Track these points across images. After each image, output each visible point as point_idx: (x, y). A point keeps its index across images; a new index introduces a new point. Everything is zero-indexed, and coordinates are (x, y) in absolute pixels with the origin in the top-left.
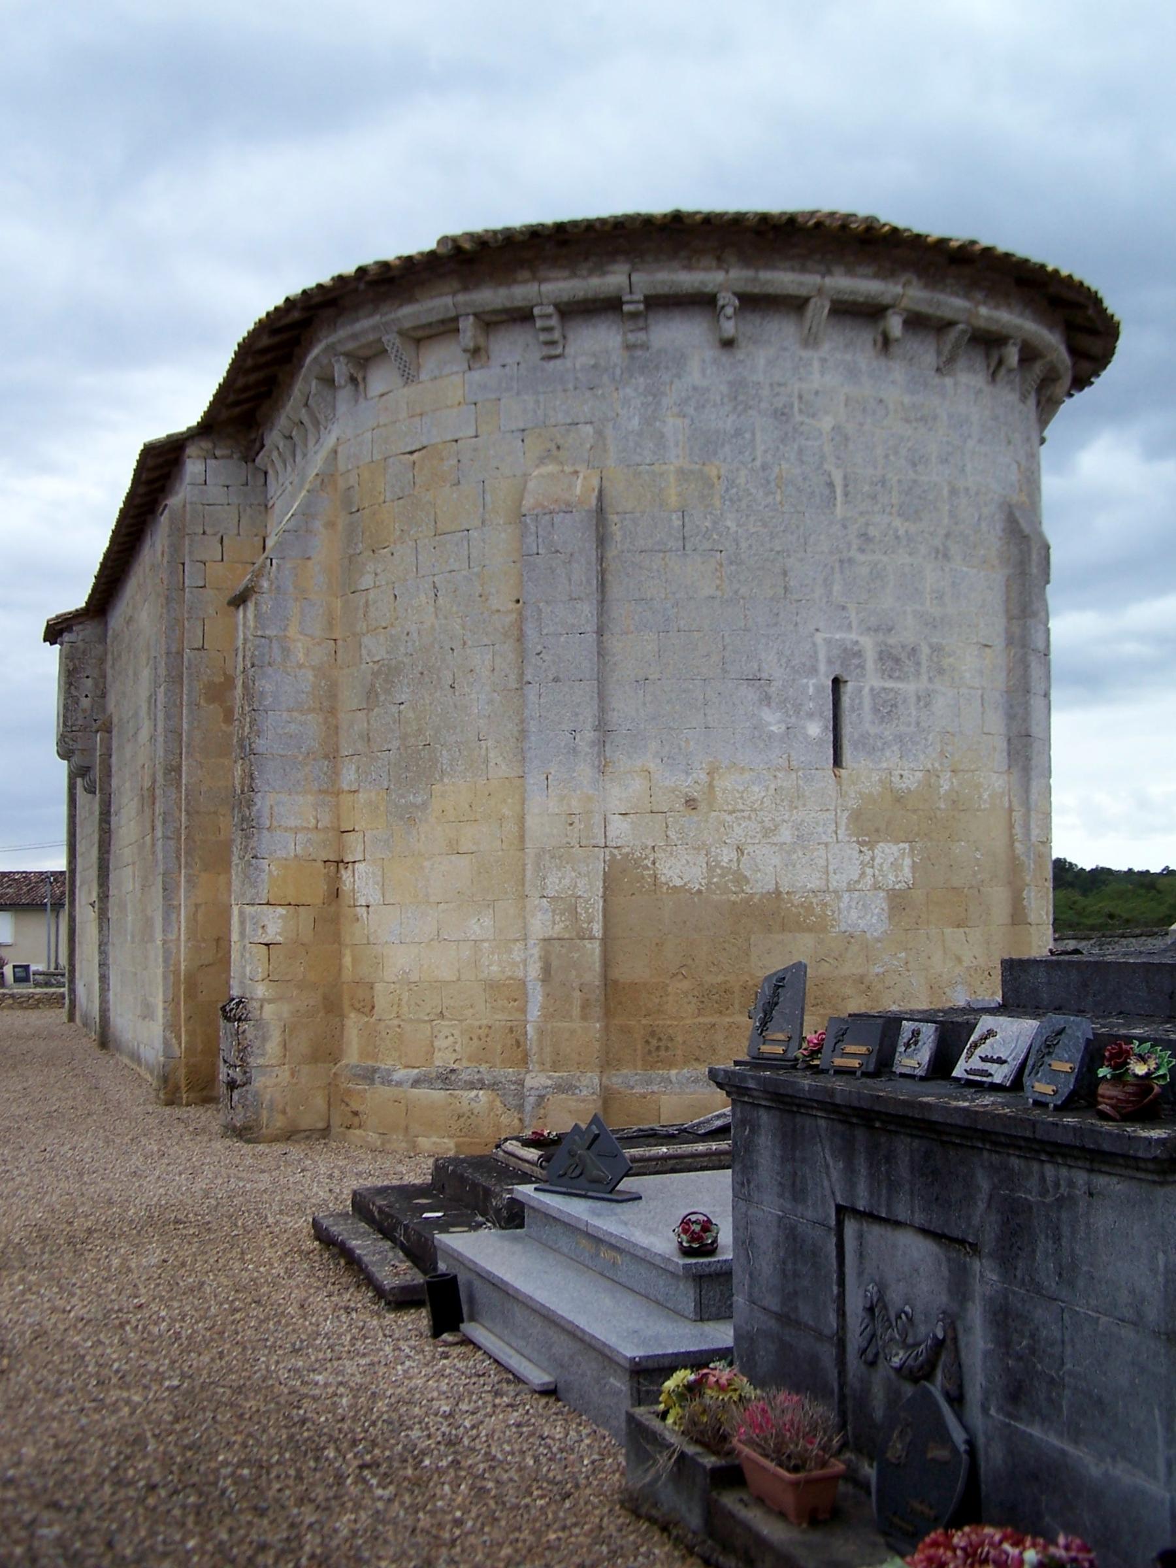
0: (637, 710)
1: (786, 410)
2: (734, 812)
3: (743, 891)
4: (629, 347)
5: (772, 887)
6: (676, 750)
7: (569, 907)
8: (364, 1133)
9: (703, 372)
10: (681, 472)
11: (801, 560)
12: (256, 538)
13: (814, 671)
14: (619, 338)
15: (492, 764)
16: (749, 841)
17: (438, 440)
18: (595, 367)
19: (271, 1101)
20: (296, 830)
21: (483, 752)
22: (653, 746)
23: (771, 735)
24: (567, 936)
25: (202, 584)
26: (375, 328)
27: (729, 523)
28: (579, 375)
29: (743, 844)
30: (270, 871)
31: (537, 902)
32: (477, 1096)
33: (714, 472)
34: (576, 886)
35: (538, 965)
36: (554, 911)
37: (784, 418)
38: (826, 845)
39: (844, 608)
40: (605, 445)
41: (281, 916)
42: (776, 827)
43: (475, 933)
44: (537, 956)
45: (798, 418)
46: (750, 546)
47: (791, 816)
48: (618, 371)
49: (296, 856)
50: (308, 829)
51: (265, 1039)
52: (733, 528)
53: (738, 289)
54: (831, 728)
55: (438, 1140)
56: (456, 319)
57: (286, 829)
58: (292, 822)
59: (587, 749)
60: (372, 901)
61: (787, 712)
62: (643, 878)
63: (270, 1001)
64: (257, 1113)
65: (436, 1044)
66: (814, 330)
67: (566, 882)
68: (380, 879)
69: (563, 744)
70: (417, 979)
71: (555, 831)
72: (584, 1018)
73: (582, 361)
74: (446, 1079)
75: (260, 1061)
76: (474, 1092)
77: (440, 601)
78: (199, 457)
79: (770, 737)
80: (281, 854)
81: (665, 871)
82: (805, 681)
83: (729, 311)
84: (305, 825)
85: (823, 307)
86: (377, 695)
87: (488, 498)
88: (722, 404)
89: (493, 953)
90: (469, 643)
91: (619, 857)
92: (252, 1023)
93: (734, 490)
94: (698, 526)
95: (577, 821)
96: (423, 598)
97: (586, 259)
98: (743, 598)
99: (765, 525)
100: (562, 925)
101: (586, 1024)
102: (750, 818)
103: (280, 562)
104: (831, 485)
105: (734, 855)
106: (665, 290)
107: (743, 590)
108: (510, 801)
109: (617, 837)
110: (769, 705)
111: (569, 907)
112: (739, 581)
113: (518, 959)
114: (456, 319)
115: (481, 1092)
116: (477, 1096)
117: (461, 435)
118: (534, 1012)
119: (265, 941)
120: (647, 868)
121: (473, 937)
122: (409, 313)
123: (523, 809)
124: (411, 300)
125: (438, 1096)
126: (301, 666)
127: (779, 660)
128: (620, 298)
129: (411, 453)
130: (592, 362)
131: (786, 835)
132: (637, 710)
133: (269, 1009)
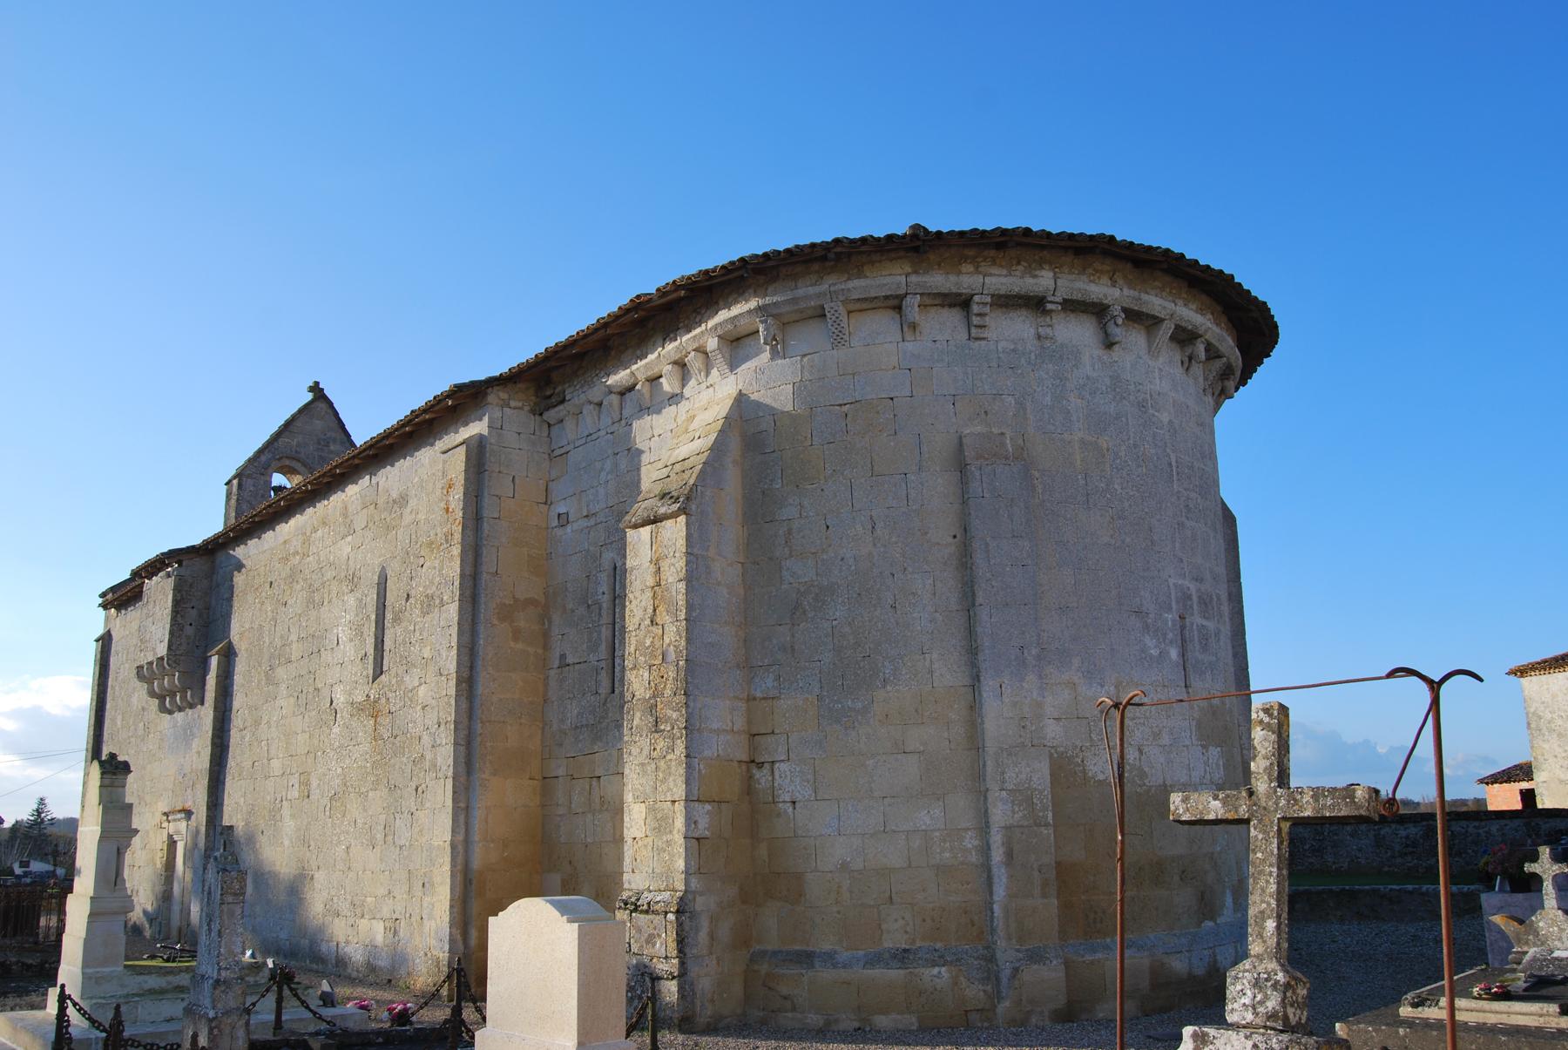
0: (1062, 631)
1: (1145, 404)
2: (1134, 719)
3: (1144, 784)
4: (1039, 337)
5: (1161, 781)
6: (1093, 666)
7: (1023, 796)
8: (799, 1016)
9: (1093, 365)
10: (1082, 441)
11: (1159, 521)
12: (541, 481)
13: (1170, 609)
14: (1032, 331)
15: (936, 674)
16: (1145, 743)
17: (874, 396)
18: (1014, 350)
19: (702, 989)
20: (718, 732)
21: (927, 663)
22: (1076, 662)
23: (1151, 657)
24: (1026, 823)
25: (496, 515)
26: (819, 295)
27: (1116, 486)
28: (1001, 355)
29: (1142, 745)
30: (699, 770)
31: (997, 794)
32: (940, 972)
33: (1105, 446)
34: (1031, 780)
35: (1001, 851)
36: (1013, 802)
37: (1143, 409)
38: (1187, 746)
39: (1182, 561)
40: (1025, 414)
41: (708, 812)
42: (1160, 731)
43: (925, 824)
44: (1000, 842)
45: (1151, 411)
46: (1130, 505)
47: (1167, 723)
48: (1033, 357)
49: (718, 755)
50: (727, 731)
51: (697, 931)
52: (1119, 491)
53: (1124, 305)
54: (451, 666)
55: (899, 1017)
56: (902, 297)
57: (711, 731)
58: (715, 726)
59: (1034, 662)
60: (799, 797)
61: (1159, 639)
62: (1075, 773)
63: (702, 894)
64: (693, 1003)
65: (884, 926)
66: (1159, 346)
67: (1023, 776)
68: (810, 777)
69: (1013, 657)
70: (861, 867)
71: (1011, 732)
72: (1044, 896)
73: (1001, 345)
74: (902, 957)
75: (694, 951)
76: (936, 970)
77: (878, 532)
78: (497, 405)
79: (1151, 659)
80: (707, 753)
81: (1092, 767)
82: (1166, 615)
83: (1120, 321)
84: (724, 727)
85: (1170, 328)
86: (804, 612)
87: (925, 449)
88: (1107, 393)
89: (945, 841)
90: (910, 569)
91: (1056, 755)
92: (688, 914)
93: (1118, 461)
94: (1096, 487)
95: (1028, 724)
96: (859, 528)
97: (1018, 263)
98: (1129, 546)
99: (1138, 491)
100: (1021, 814)
101: (1046, 901)
102: (1144, 724)
103: (703, 489)
104: (1170, 464)
105: (1137, 754)
106: (1077, 296)
107: (1128, 540)
108: (956, 706)
109: (1054, 738)
110: (1148, 633)
111: (1023, 796)
112: (1125, 533)
113: (970, 846)
114: (902, 297)
115: (943, 969)
116: (940, 972)
117: (897, 394)
118: (1000, 892)
119: (696, 836)
120: (1079, 765)
121: (924, 827)
122: (859, 286)
123: (225, 707)
124: (860, 275)
125: (895, 974)
126: (719, 584)
127: (1152, 597)
128: (1045, 297)
129: (840, 405)
130: (1012, 347)
131: (1166, 739)
132: (1062, 631)
133: (700, 900)
